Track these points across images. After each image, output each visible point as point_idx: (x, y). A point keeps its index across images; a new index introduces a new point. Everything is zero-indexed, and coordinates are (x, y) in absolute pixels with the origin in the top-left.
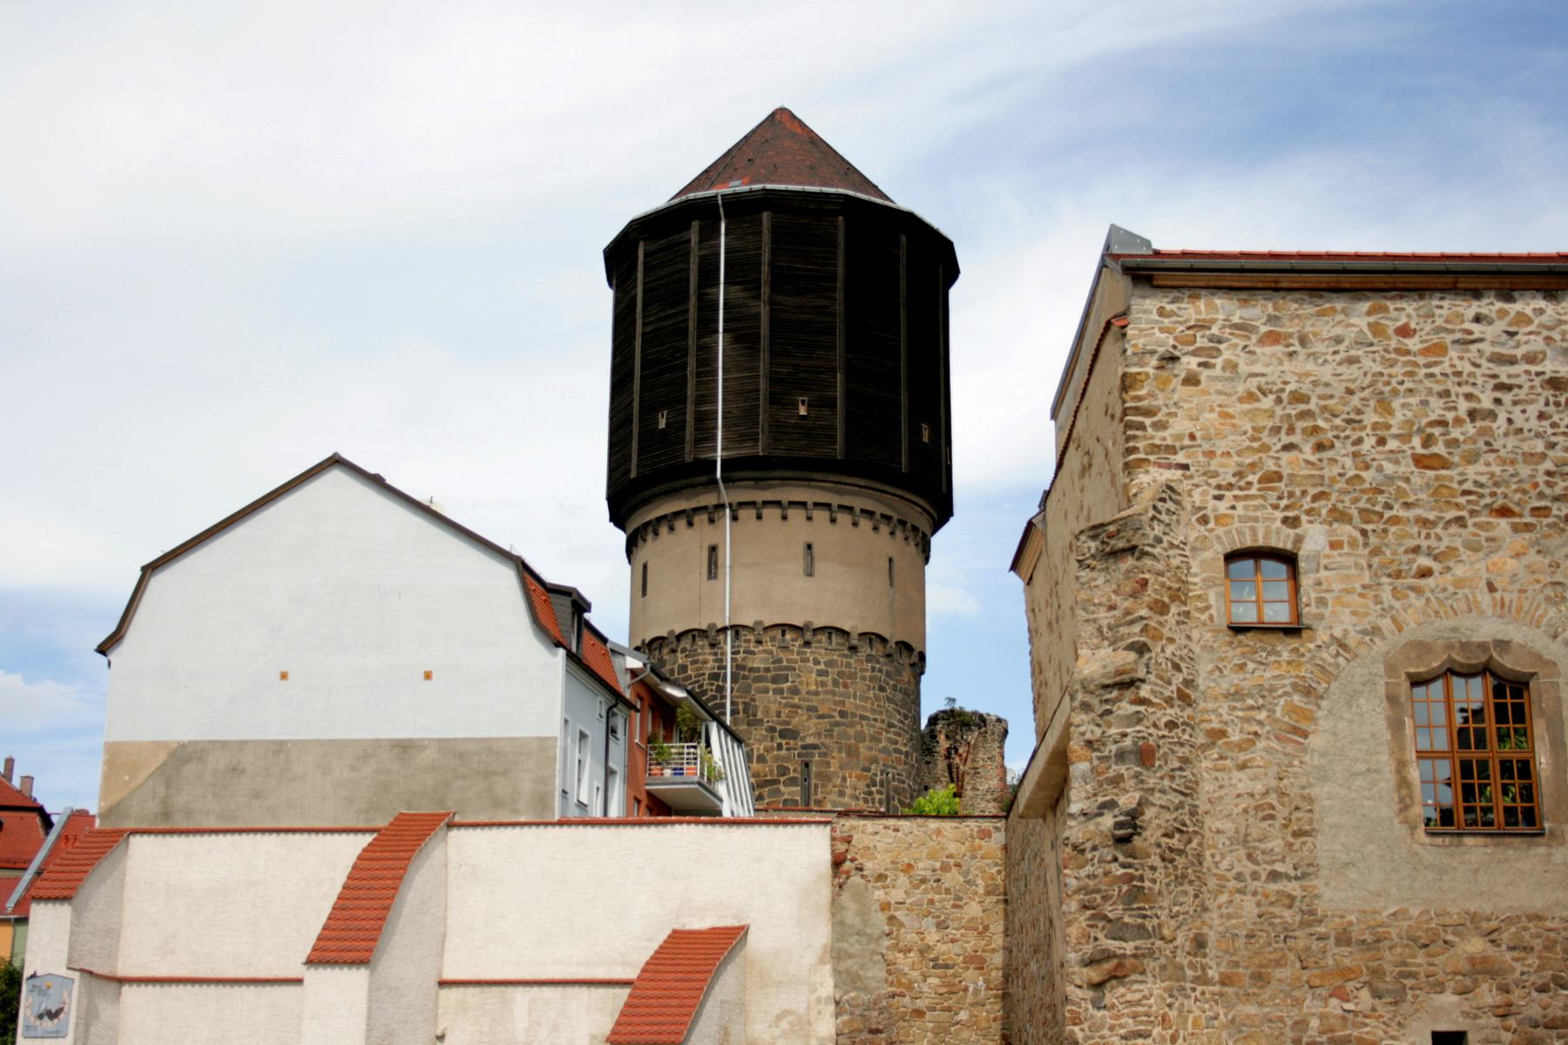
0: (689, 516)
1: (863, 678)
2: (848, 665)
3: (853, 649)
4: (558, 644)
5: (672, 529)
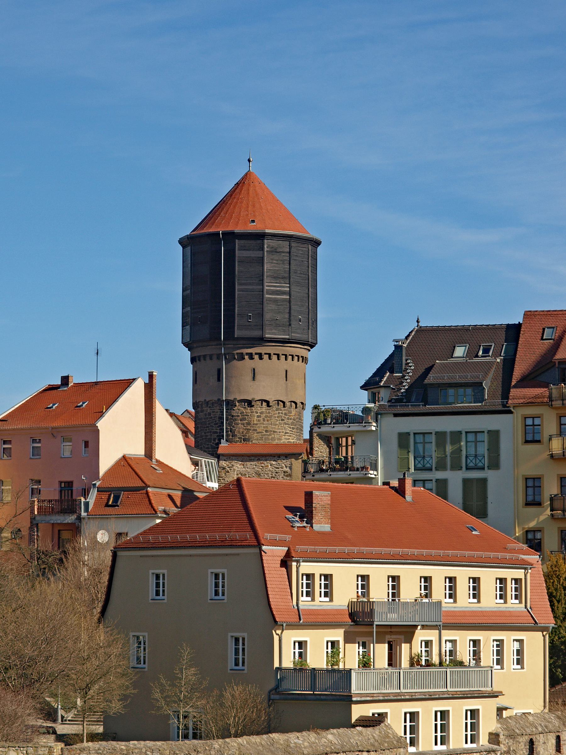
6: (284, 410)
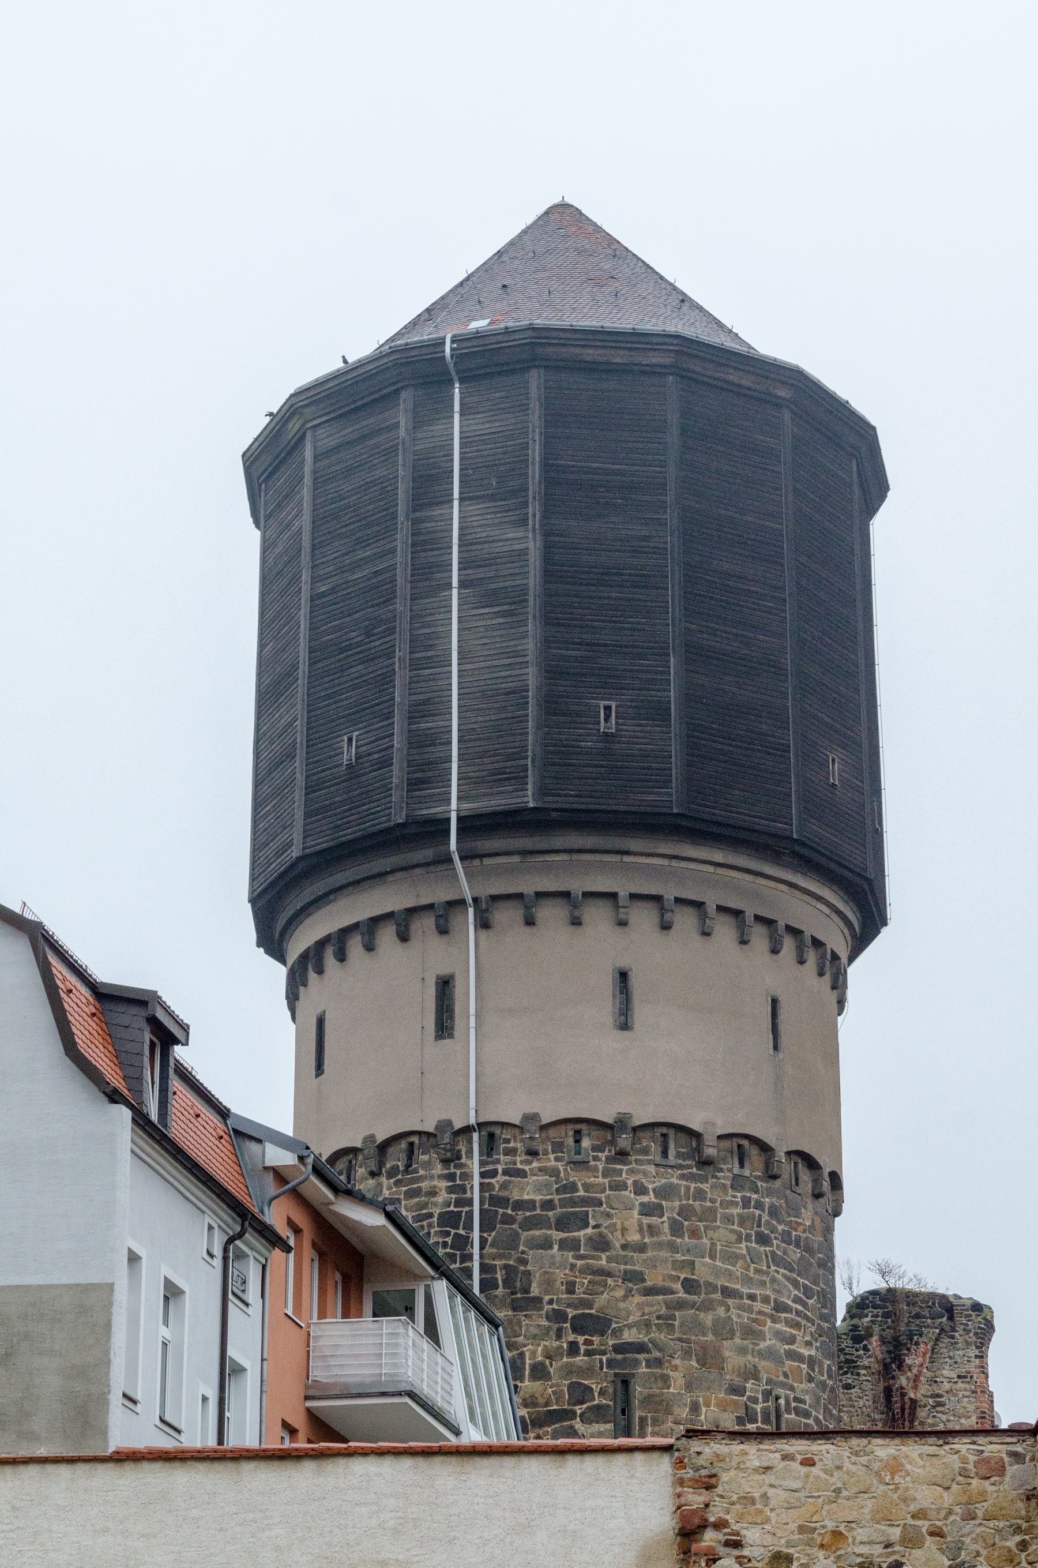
0: (403, 923)
1: (729, 1219)
2: (700, 1195)
3: (706, 1163)
4: (114, 1097)
5: (370, 947)
6: (770, 1193)
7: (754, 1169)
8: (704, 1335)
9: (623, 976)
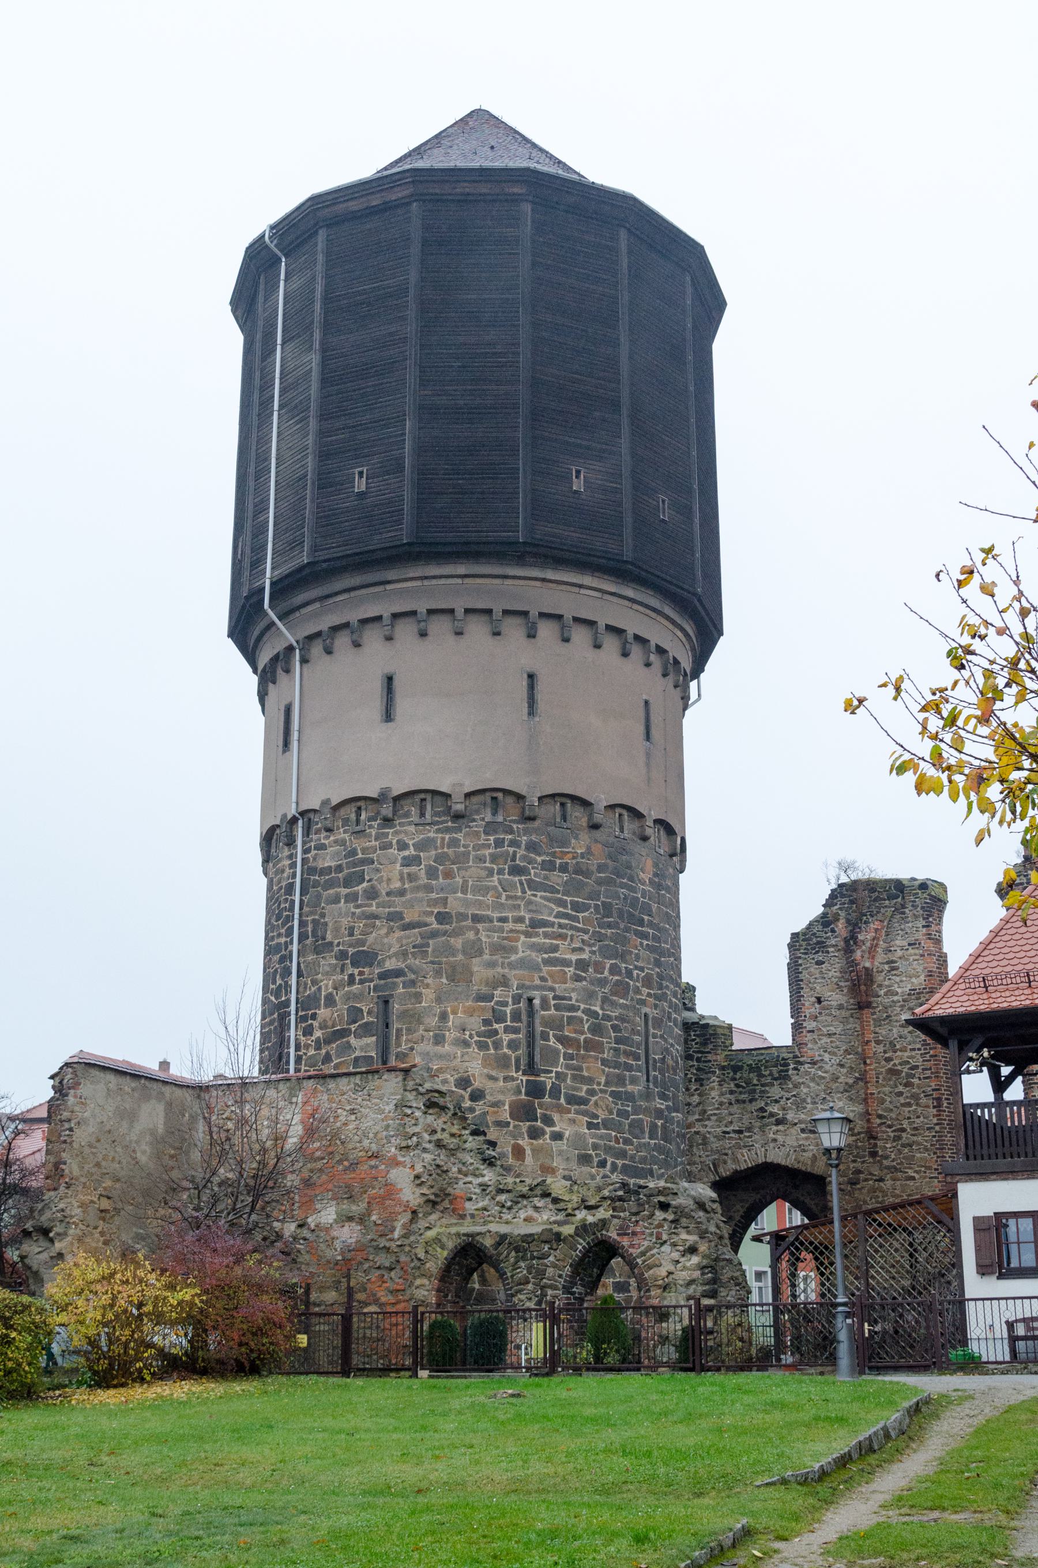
1: (481, 859)
2: (454, 843)
3: (458, 817)
6: (526, 832)
7: (510, 813)
8: (454, 955)
9: (390, 679)
